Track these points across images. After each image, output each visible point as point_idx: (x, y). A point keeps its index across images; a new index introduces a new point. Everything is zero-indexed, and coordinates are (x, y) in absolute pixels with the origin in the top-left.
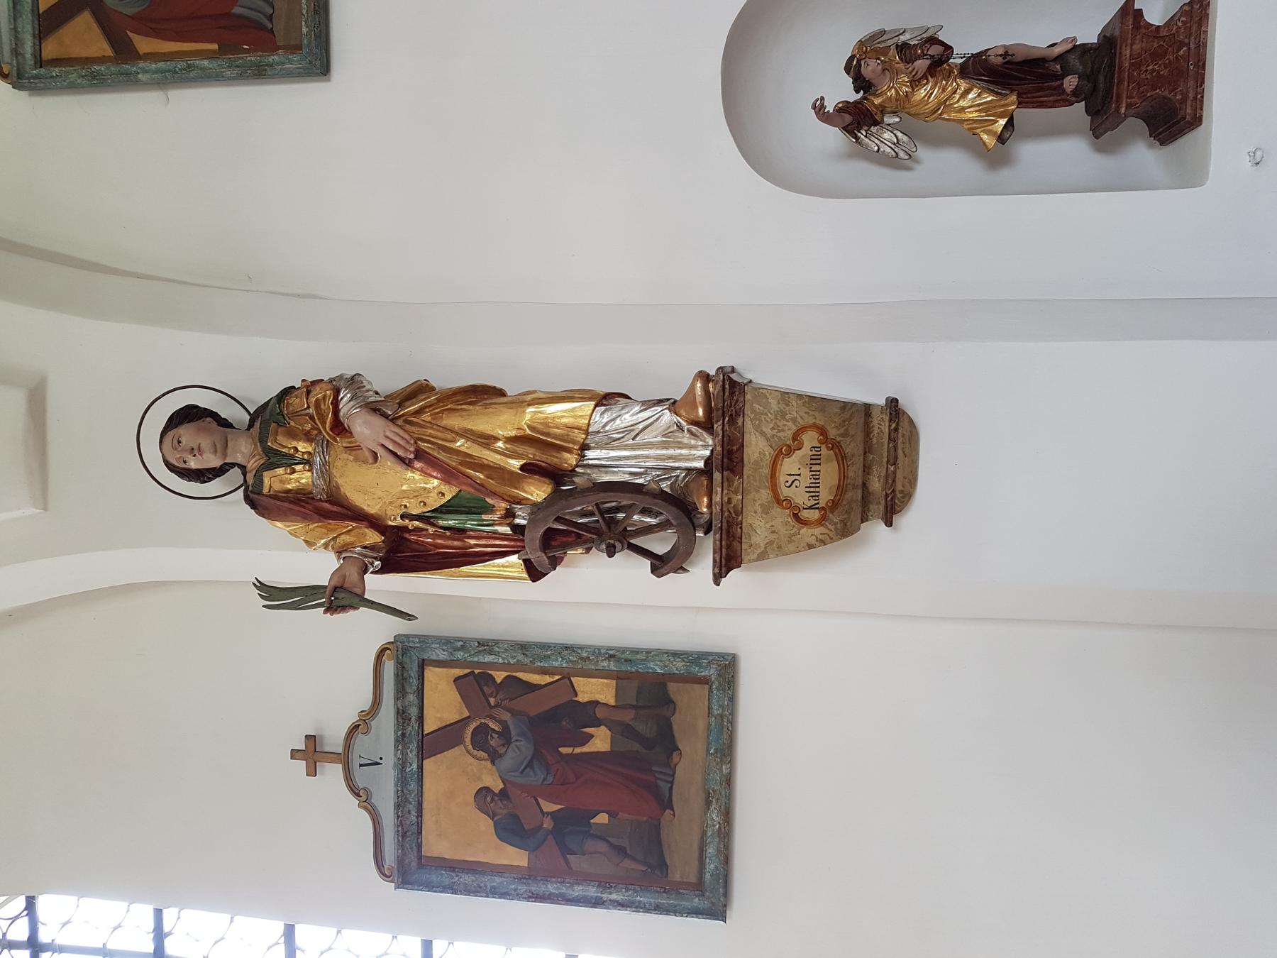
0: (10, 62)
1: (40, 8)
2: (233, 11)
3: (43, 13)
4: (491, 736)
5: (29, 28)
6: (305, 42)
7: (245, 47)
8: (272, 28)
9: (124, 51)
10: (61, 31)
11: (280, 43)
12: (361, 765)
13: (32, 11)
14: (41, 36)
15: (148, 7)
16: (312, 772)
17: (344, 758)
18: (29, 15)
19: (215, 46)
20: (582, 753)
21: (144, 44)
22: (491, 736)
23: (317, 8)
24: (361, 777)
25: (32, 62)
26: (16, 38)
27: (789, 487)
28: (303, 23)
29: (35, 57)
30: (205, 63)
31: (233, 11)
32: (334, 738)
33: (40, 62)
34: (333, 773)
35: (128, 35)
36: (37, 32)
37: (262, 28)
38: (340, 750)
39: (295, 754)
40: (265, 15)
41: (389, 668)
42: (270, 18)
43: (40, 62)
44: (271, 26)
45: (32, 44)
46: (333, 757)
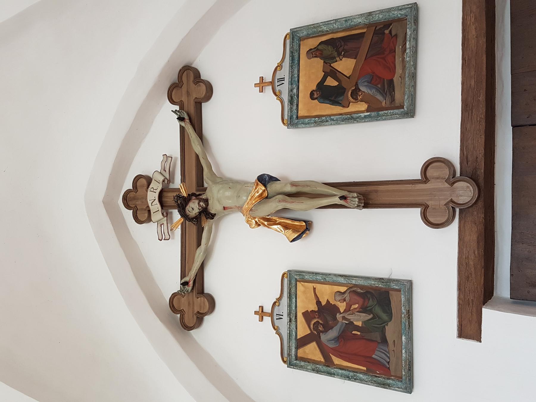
0: (287, 357)
1: (298, 337)
2: (373, 356)
3: (298, 339)
4: (320, 326)
5: (294, 345)
6: (404, 378)
7: (377, 372)
8: (389, 367)
9: (328, 362)
10: (305, 347)
11: (392, 374)
12: (277, 319)
13: (295, 339)
14: (297, 348)
15: (338, 346)
16: (261, 91)
17: (271, 315)
18: (294, 340)
19: (365, 369)
20: (363, 367)
21: (337, 361)
22: (320, 326)
23: (410, 368)
24: (277, 323)
25: (294, 358)
26: (290, 349)
27: (263, 87)
28: (403, 370)
29: (295, 356)
30: (361, 376)
31: (373, 356)
32: (268, 309)
33: (297, 358)
34: (267, 320)
35: (330, 355)
36: (296, 346)
37: (384, 366)
38: (270, 312)
39: (256, 313)
40: (386, 361)
41: (286, 281)
42: (388, 363)
43: (297, 358)
44: (389, 366)
45: (294, 351)
46: (267, 314)
